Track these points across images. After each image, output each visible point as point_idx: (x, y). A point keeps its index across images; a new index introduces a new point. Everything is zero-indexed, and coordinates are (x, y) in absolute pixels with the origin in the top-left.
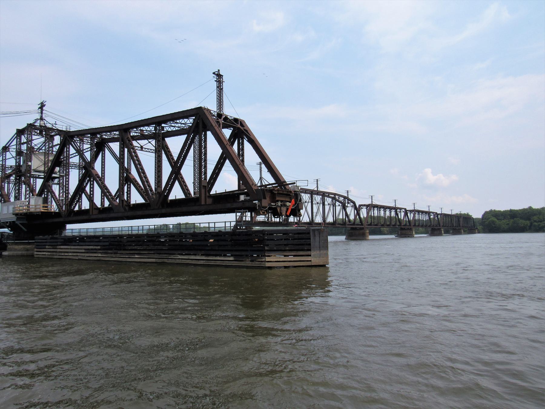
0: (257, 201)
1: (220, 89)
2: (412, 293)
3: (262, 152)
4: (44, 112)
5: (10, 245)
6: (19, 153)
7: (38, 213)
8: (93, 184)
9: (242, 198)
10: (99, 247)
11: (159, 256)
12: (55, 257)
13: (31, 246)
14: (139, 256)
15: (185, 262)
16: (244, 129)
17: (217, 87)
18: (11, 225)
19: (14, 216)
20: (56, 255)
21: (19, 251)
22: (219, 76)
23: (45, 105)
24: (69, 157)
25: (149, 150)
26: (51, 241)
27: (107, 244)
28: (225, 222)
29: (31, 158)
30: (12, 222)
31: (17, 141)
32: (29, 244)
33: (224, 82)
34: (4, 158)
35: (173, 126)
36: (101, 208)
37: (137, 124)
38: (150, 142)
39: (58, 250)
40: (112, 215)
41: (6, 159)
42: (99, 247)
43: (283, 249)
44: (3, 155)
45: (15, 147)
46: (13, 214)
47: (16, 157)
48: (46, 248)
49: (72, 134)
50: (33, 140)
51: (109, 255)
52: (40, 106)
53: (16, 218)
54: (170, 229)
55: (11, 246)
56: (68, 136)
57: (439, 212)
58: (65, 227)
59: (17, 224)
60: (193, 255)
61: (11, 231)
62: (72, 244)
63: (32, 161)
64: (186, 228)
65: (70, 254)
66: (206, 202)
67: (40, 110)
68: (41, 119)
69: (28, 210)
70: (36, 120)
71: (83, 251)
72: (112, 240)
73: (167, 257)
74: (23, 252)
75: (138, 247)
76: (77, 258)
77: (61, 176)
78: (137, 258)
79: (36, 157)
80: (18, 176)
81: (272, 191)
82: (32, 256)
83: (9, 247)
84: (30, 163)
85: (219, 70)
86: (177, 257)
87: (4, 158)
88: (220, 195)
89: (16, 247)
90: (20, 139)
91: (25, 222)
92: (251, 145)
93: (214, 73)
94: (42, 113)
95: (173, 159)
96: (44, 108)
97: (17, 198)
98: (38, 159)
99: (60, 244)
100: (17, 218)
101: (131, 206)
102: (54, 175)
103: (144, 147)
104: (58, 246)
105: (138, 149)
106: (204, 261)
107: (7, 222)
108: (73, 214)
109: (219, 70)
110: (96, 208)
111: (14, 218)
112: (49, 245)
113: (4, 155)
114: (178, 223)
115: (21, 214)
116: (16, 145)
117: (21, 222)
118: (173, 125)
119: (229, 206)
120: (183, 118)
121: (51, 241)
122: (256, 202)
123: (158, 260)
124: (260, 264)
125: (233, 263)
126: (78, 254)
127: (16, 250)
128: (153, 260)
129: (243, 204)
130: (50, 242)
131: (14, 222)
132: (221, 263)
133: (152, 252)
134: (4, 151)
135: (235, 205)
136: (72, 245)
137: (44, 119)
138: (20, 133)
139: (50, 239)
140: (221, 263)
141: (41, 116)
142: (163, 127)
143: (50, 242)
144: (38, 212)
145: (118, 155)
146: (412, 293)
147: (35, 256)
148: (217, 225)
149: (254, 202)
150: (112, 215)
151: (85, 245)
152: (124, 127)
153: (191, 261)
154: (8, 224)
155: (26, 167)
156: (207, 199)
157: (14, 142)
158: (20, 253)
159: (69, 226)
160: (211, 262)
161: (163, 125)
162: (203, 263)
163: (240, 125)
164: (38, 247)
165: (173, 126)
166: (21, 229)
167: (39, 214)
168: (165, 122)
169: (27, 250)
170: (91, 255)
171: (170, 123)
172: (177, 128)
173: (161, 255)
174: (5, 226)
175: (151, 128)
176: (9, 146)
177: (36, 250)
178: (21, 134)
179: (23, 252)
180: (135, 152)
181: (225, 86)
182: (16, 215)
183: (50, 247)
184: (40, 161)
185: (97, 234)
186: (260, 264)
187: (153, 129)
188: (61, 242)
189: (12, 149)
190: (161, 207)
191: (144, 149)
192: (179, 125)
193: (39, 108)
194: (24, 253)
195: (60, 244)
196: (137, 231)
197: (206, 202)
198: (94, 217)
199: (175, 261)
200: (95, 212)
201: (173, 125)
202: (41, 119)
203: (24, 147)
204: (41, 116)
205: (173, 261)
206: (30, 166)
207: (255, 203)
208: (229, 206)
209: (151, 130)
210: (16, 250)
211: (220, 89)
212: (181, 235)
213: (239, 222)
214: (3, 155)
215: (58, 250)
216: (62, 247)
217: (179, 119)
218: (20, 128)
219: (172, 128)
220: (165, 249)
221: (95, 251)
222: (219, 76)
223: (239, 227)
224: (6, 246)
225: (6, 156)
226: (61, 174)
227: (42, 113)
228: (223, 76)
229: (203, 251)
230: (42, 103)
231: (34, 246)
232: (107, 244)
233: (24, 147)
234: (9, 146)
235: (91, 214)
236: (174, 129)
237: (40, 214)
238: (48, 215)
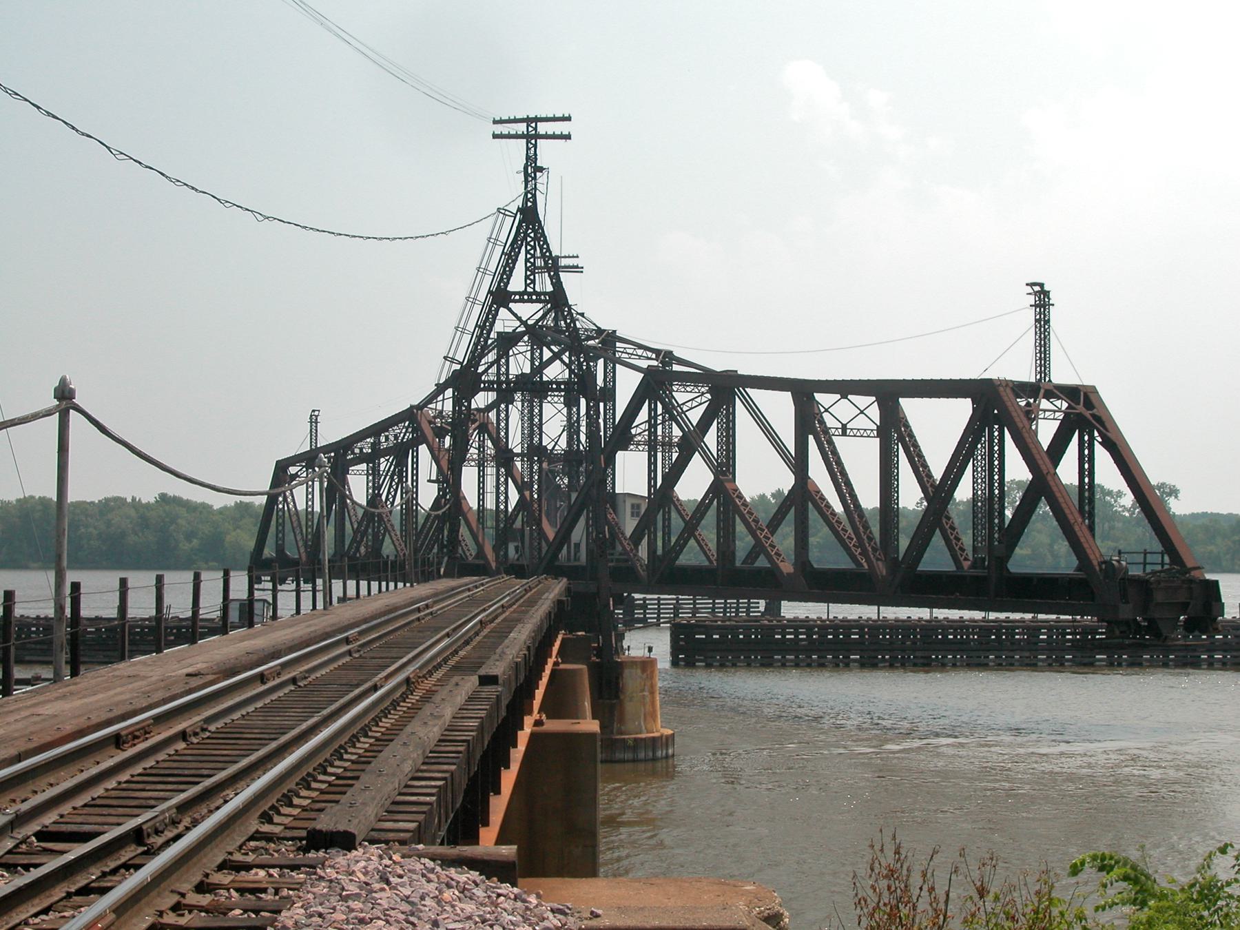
2: (1172, 687)
3: (163, 869)
8: (669, 512)
16: (1094, 416)
17: (1036, 320)
22: (1042, 299)
25: (861, 434)
33: (1053, 305)
64: (862, 412)
92: (1108, 453)
95: (930, 476)
102: (1179, 624)
105: (836, 433)
145: (792, 448)
146: (1172, 687)
163: (1085, 405)
180: (831, 443)
181: (1055, 314)
191: (848, 431)
222: (1042, 299)
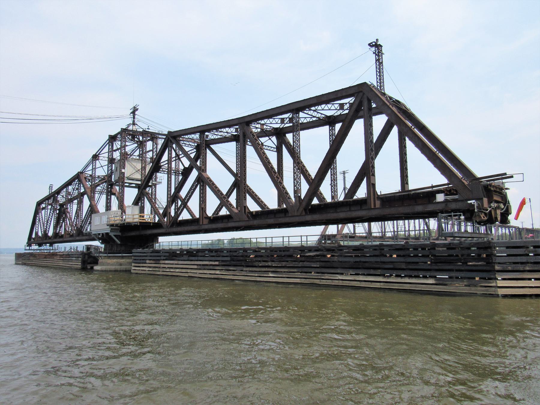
0: (474, 201)
1: (379, 62)
4: (136, 116)
5: (102, 259)
6: (111, 161)
7: (136, 224)
9: (440, 198)
10: (217, 263)
11: (306, 275)
12: (158, 273)
13: (124, 260)
14: (274, 274)
15: (349, 284)
18: (105, 238)
19: (108, 227)
20: (160, 271)
21: (112, 265)
22: (376, 46)
23: (137, 109)
24: (171, 160)
26: (152, 254)
27: (229, 259)
28: (301, 236)
29: (124, 165)
30: (105, 234)
31: (109, 148)
32: (123, 257)
34: (94, 167)
35: (215, 135)
36: (212, 217)
37: (218, 126)
38: (270, 139)
39: (162, 266)
40: (231, 224)
41: (95, 169)
42: (217, 263)
43: (521, 269)
44: (93, 163)
45: (107, 155)
46: (108, 225)
47: (108, 165)
48: (146, 263)
49: (175, 134)
50: (127, 146)
51: (231, 273)
52: (131, 111)
53: (110, 229)
54: (224, 244)
55: (104, 260)
56: (171, 137)
57: (521, 227)
58: (158, 239)
59: (110, 236)
60: (362, 275)
61: (102, 243)
62: (179, 259)
63: (126, 168)
65: (177, 270)
66: (203, 223)
67: (132, 115)
68: (134, 124)
69: (122, 220)
70: (129, 125)
71: (196, 267)
72: (283, 254)
73: (319, 277)
74: (117, 267)
75: (273, 263)
76: (186, 275)
77: (154, 184)
78: (271, 277)
79: (129, 164)
80: (109, 185)
81: (488, 187)
82: (128, 271)
83: (100, 260)
84: (123, 171)
85: (377, 40)
86: (338, 277)
87: (94, 167)
88: (392, 196)
89: (109, 261)
90: (112, 146)
91: (119, 234)
93: (369, 45)
94: (134, 118)
96: (136, 113)
97: (108, 207)
98: (131, 166)
99: (165, 258)
100: (112, 229)
101: (254, 214)
103: (264, 144)
104: (161, 261)
106: (382, 284)
107: (99, 234)
108: (141, 227)
109: (377, 40)
110: (206, 216)
111: (107, 230)
112: (150, 260)
113: (94, 164)
114: (233, 238)
115: (117, 225)
116: (108, 152)
117: (115, 234)
118: (216, 133)
119: (419, 208)
120: (190, 134)
121: (152, 254)
122: (472, 202)
123: (303, 281)
124: (487, 291)
125: (434, 288)
126: (189, 271)
127: (108, 264)
128: (298, 281)
129: (446, 205)
130: (151, 256)
131: (107, 234)
132: (411, 287)
133: (295, 270)
134: (94, 159)
135: (430, 208)
136: (179, 260)
137: (136, 124)
138: (112, 139)
139: (151, 253)
140: (411, 287)
141: (134, 121)
142: (207, 136)
143: (151, 256)
144: (135, 222)
147: (132, 271)
148: (275, 240)
149: (469, 202)
150: (231, 224)
151: (197, 260)
152: (247, 120)
153: (359, 283)
154: (100, 236)
155: (120, 174)
156: (204, 219)
157: (106, 149)
158: (113, 268)
159: (161, 239)
160: (394, 286)
161: (207, 133)
162: (380, 287)
164: (136, 261)
165: (215, 135)
166: (114, 241)
167: (137, 225)
168: (209, 131)
169: (121, 265)
170: (205, 272)
171: (254, 124)
172: (219, 137)
173: (308, 274)
174: (96, 238)
175: (232, 129)
176: (99, 154)
177: (133, 264)
178: (113, 140)
179: (117, 267)
181: (385, 59)
182: (112, 225)
183: (151, 262)
184: (133, 167)
185: (235, 247)
186: (487, 291)
187: (234, 131)
188: (165, 256)
189: (101, 157)
190: (304, 213)
192: (222, 133)
193: (131, 113)
194: (118, 267)
195: (165, 258)
196: (255, 244)
197: (203, 223)
198: (206, 227)
199: (332, 282)
200: (206, 221)
201: (216, 133)
202: (134, 124)
203: (117, 155)
204: (134, 121)
205: (329, 282)
206: (124, 173)
207: (471, 203)
208: (419, 208)
209: (232, 132)
210: (108, 264)
211: (379, 62)
212: (382, 248)
213: (324, 237)
214: (93, 163)
215: (162, 266)
216: (167, 262)
217: (221, 128)
218: (113, 133)
219: (215, 136)
220: (315, 266)
221: (211, 267)
222: (376, 46)
223: (323, 242)
224: (98, 260)
225: (95, 165)
226: (153, 182)
227: (134, 118)
228: (382, 46)
229: (380, 270)
230: (134, 107)
231: (131, 260)
232: (229, 259)
233: (117, 155)
234: (99, 154)
235: (201, 224)
236: (217, 137)
237: (152, 225)
238: (145, 226)
